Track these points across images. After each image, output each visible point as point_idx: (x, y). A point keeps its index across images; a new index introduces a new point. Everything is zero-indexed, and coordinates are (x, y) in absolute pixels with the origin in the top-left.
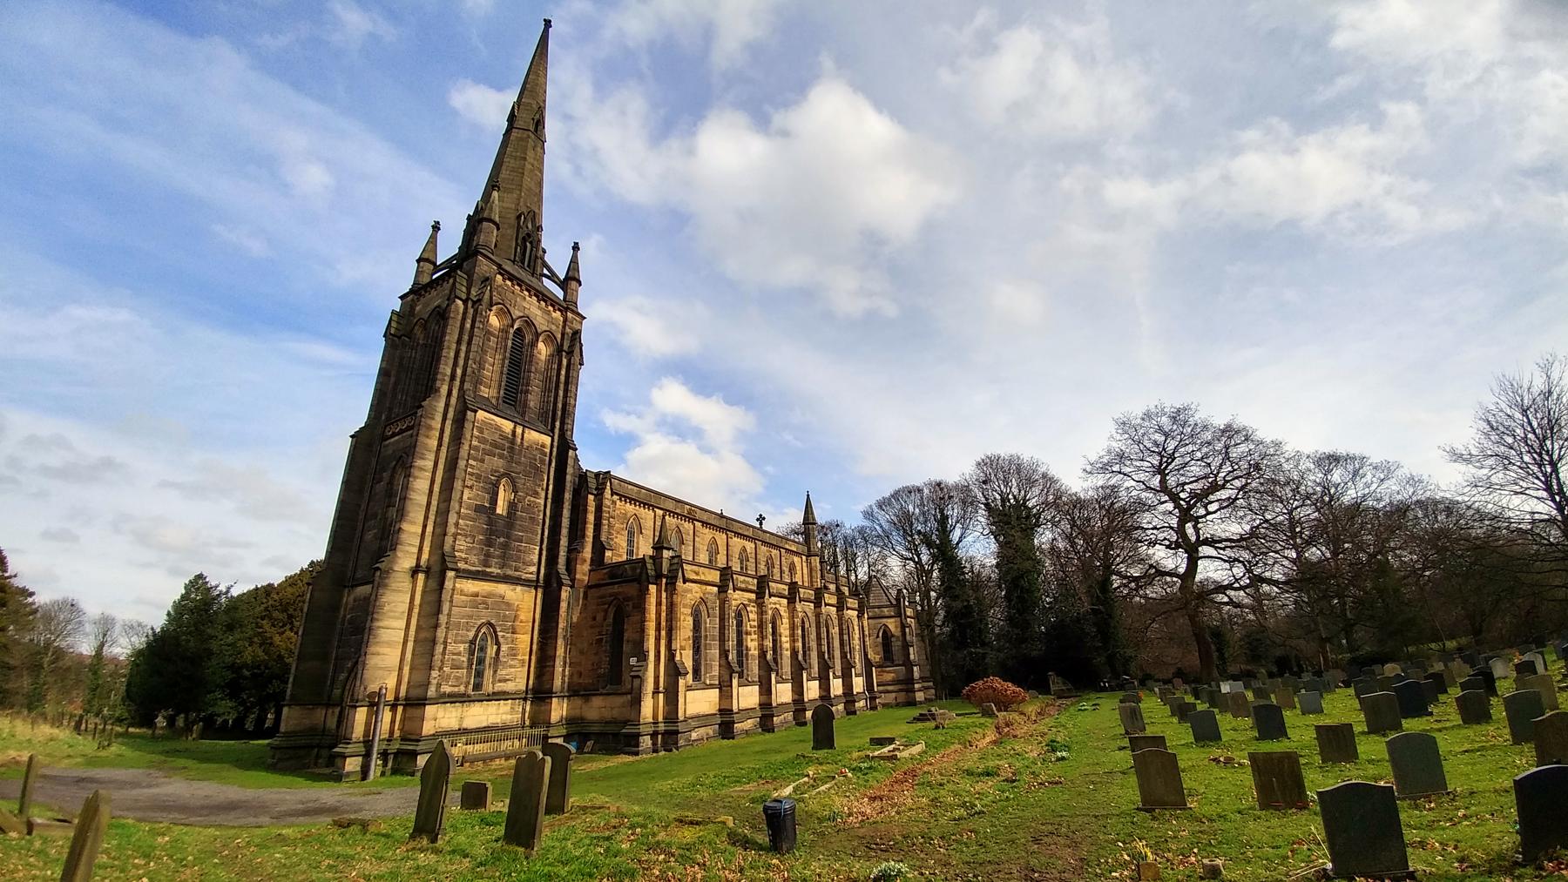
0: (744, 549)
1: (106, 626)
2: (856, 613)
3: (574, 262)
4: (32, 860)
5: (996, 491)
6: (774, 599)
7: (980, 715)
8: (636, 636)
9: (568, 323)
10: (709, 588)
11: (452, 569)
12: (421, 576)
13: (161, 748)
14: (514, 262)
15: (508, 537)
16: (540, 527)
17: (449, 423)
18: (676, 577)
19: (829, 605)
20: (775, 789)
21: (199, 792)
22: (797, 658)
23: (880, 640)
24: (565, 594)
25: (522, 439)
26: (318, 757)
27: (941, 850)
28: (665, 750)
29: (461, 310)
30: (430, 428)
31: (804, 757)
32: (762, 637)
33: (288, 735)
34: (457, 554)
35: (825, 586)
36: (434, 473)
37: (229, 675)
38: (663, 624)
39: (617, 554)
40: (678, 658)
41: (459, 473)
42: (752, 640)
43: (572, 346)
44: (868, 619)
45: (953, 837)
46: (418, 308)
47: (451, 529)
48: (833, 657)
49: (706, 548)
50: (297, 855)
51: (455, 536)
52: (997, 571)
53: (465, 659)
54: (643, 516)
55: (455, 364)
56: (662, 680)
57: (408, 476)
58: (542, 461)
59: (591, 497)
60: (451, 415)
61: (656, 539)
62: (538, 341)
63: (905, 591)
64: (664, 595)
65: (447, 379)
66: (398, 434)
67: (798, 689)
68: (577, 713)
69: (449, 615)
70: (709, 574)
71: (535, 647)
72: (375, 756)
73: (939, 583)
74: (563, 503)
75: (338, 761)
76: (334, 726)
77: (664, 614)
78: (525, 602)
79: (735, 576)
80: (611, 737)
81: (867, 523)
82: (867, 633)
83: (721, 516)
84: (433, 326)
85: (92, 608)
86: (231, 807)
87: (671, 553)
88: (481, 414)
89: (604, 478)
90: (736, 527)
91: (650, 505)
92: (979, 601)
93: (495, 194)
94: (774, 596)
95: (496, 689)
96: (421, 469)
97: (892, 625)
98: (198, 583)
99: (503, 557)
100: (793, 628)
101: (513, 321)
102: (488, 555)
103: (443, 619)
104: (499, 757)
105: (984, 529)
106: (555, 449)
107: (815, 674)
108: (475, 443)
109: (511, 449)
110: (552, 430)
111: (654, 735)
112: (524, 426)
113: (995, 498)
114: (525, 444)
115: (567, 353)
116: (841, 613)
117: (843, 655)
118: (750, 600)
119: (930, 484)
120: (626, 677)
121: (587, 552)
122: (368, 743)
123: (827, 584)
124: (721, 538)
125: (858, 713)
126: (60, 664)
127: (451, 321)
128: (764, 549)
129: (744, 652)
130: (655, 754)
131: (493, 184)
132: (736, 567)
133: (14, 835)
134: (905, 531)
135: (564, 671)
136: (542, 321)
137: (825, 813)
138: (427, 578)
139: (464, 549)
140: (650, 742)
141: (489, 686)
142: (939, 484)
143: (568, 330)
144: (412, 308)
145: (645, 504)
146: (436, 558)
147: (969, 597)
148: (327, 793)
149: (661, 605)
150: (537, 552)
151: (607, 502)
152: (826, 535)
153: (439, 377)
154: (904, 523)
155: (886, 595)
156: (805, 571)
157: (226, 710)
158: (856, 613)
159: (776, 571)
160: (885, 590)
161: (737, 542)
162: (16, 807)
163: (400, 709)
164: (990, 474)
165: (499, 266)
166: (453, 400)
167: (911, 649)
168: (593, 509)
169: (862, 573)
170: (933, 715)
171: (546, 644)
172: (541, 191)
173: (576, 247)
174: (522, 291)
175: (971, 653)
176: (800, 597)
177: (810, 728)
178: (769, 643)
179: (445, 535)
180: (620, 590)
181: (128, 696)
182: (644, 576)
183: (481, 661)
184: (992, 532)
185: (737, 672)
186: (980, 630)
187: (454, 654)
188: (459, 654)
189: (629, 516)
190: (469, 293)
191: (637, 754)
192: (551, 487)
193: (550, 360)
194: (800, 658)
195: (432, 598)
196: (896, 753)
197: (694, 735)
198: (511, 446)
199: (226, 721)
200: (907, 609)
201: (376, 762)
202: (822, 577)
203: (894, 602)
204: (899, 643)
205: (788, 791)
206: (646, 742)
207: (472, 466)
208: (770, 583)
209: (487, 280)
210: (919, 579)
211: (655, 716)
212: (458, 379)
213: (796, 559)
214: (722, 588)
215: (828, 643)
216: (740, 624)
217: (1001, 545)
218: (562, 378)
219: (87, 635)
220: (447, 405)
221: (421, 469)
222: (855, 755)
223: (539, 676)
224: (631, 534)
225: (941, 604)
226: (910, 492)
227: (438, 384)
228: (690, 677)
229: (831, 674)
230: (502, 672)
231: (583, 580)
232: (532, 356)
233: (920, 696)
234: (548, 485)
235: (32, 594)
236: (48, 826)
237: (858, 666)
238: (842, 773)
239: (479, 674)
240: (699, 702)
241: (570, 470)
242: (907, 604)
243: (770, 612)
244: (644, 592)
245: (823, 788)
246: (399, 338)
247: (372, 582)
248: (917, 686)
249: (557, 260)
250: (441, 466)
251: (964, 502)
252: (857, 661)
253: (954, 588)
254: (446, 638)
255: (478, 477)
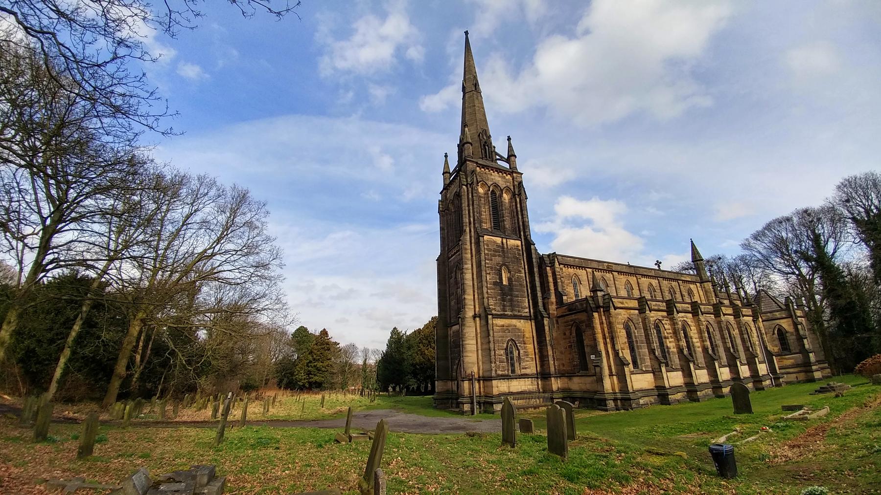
0: (651, 284)
1: (366, 351)
2: (751, 318)
3: (510, 147)
4: (352, 453)
5: (859, 205)
6: (681, 315)
7: (871, 384)
8: (592, 343)
9: (515, 179)
10: (632, 311)
11: (490, 314)
12: (477, 319)
13: (393, 400)
14: (482, 158)
15: (511, 295)
16: (526, 288)
17: (473, 245)
18: (609, 307)
19: (727, 315)
20: (712, 438)
21: (410, 419)
22: (708, 353)
23: (776, 335)
24: (546, 322)
25: (507, 245)
26: (452, 403)
27: (851, 477)
28: (624, 409)
29: (466, 190)
30: (466, 249)
31: (729, 418)
32: (678, 340)
33: (439, 393)
34: (491, 307)
35: (719, 301)
36: (472, 270)
37: (412, 368)
38: (607, 335)
39: (570, 297)
40: (621, 355)
41: (483, 268)
42: (670, 342)
43: (520, 191)
44: (762, 321)
45: (859, 469)
46: (448, 196)
47: (486, 295)
48: (738, 351)
49: (624, 287)
50: (456, 448)
51: (488, 298)
52: (871, 270)
53: (505, 358)
54: (580, 274)
55: (469, 216)
56: (613, 368)
57: (462, 273)
58: (519, 254)
59: (548, 268)
60: (473, 241)
61: (591, 286)
62: (502, 193)
63: (791, 298)
64: (604, 318)
65: (468, 224)
66: (454, 255)
67: (713, 373)
68: (566, 386)
69: (493, 337)
70: (631, 302)
71: (537, 351)
72: (475, 404)
73: (822, 288)
74: (534, 274)
75: (461, 405)
76: (456, 390)
77: (606, 329)
78: (527, 327)
79: (648, 302)
80: (588, 400)
81: (747, 252)
82: (763, 331)
83: (629, 266)
84: (456, 202)
85: (360, 347)
86: (424, 425)
87: (603, 293)
88: (486, 237)
89: (553, 256)
90: (641, 271)
91: (582, 267)
92: (860, 296)
93: (466, 129)
94: (681, 312)
95: (522, 373)
96: (467, 269)
97: (786, 324)
98: (395, 331)
99: (511, 305)
100: (700, 332)
101: (489, 187)
102: (504, 306)
103: (491, 339)
104: (531, 407)
105: (855, 238)
106: (524, 247)
107: (724, 362)
108: (486, 252)
109: (503, 251)
110: (520, 237)
111: (615, 400)
112: (507, 238)
113: (859, 212)
114: (509, 247)
115: (518, 195)
116: (739, 319)
117: (746, 349)
118: (663, 317)
119: (798, 213)
120: (590, 366)
121: (553, 298)
122: (472, 398)
123: (722, 301)
124: (633, 280)
125: (765, 389)
126: (352, 369)
127: (463, 197)
128: (665, 282)
129: (666, 350)
130: (618, 412)
131: (464, 125)
132: (648, 297)
133: (344, 443)
134: (782, 253)
135: (554, 363)
136: (503, 183)
137: (755, 455)
138: (480, 320)
139: (493, 304)
140: (613, 404)
141: (518, 372)
142: (806, 211)
143: (516, 183)
144: (446, 196)
145: (579, 267)
146: (481, 310)
147: (851, 295)
148: (460, 421)
149: (603, 324)
150: (527, 301)
151: (557, 270)
152: (712, 266)
153: (464, 224)
154: (781, 246)
155: (776, 303)
156: (701, 293)
157: (413, 384)
158: (751, 318)
159: (678, 295)
160: (773, 299)
161: (645, 281)
162: (343, 431)
163: (481, 382)
164: (851, 193)
165: (477, 163)
166: (473, 234)
167: (805, 341)
168: (551, 274)
169: (750, 289)
170: (833, 387)
171: (542, 349)
172: (486, 118)
173: (509, 139)
174: (489, 171)
175: (858, 338)
176: (723, 313)
177: (729, 400)
178: (683, 343)
179: (483, 298)
180: (576, 317)
181: (378, 380)
182: (589, 308)
183: (512, 359)
184: (862, 240)
185: (663, 363)
186: (864, 320)
187: (499, 355)
188: (501, 355)
189: (571, 275)
190: (467, 181)
191: (606, 410)
192: (526, 267)
193: (510, 202)
194: (710, 352)
195: (484, 329)
196: (806, 415)
197: (641, 401)
198: (502, 250)
199: (413, 388)
200: (796, 311)
201: (476, 406)
202: (716, 296)
203: (784, 307)
204: (794, 337)
205: (722, 440)
206: (611, 404)
207: (488, 264)
208: (676, 304)
209: (473, 172)
210: (802, 287)
211: (613, 389)
212: (472, 223)
213: (692, 286)
214: (641, 311)
215: (732, 341)
216: (659, 332)
217: (872, 249)
218: (519, 209)
219: (359, 356)
220: (471, 237)
221: (467, 269)
222: (771, 417)
223: (542, 366)
224: (575, 285)
225: (826, 304)
226: (781, 222)
227: (465, 227)
228: (631, 366)
229: (738, 363)
230: (523, 364)
231: (554, 314)
232: (502, 202)
233: (817, 375)
234: (524, 266)
235: (339, 344)
236: (357, 437)
237: (760, 356)
238: (763, 429)
239: (513, 365)
240: (641, 381)
241: (534, 256)
242: (795, 307)
243: (680, 323)
244: (590, 319)
245: (750, 439)
246: (444, 211)
247: (459, 324)
248: (814, 368)
249: (501, 148)
250: (474, 266)
251: (832, 220)
252: (758, 352)
253: (836, 289)
254: (494, 348)
255: (491, 268)
